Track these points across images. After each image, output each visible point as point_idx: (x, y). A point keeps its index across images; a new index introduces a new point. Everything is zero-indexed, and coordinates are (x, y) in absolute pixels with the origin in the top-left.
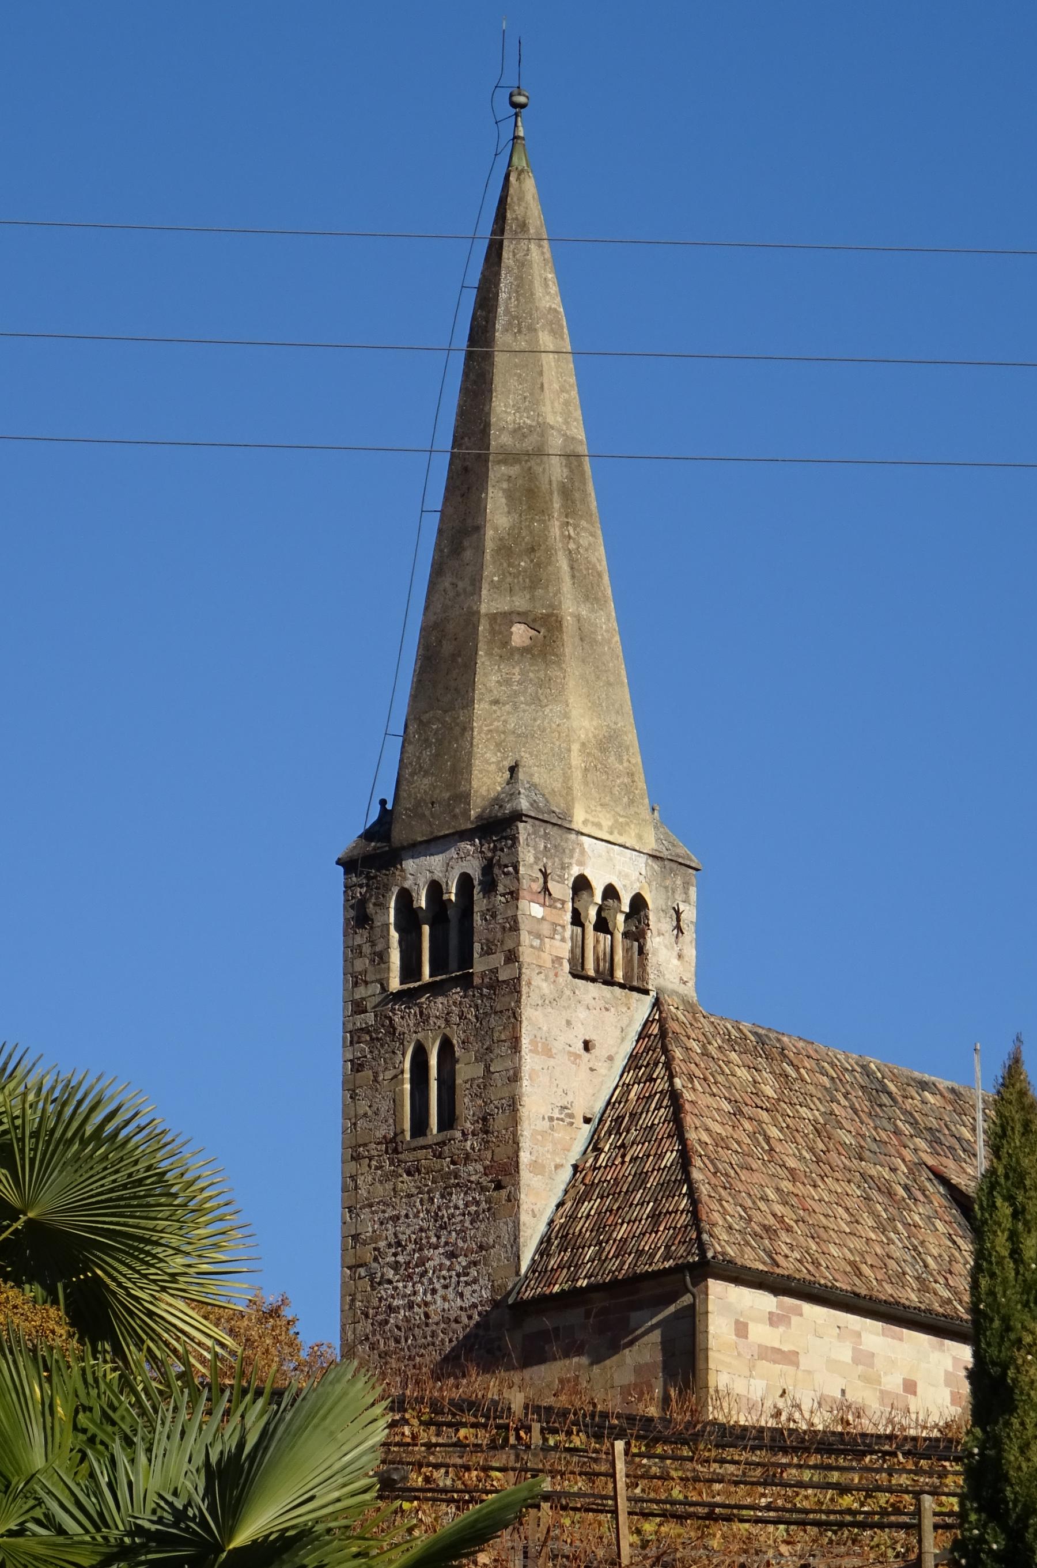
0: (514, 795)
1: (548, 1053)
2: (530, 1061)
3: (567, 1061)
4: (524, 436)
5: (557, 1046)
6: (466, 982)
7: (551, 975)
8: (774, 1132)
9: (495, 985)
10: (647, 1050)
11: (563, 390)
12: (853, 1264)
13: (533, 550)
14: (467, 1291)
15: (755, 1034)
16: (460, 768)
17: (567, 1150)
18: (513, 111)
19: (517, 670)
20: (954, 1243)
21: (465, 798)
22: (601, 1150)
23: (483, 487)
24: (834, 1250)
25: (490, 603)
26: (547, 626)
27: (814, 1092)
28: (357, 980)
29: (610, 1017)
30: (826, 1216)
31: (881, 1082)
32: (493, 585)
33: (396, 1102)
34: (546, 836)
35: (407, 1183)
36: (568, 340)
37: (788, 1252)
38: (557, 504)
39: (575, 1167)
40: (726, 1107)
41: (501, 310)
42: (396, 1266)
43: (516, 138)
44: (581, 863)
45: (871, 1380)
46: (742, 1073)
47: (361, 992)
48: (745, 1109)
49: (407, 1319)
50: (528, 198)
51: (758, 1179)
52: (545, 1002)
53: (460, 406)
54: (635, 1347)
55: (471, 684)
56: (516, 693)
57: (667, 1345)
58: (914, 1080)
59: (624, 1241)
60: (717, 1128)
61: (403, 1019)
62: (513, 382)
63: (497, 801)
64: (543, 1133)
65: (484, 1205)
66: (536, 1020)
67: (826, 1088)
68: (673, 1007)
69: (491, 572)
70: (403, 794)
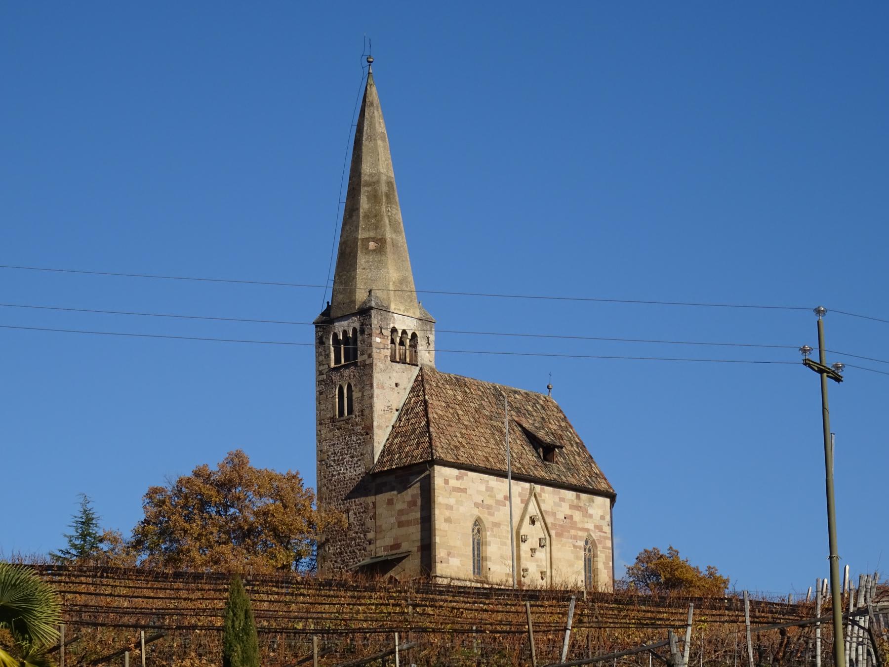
0: (370, 301)
1: (383, 388)
2: (376, 391)
3: (390, 390)
5: (387, 385)
8: (460, 412)
9: (365, 365)
16: (353, 292)
17: (390, 420)
21: (354, 302)
24: (480, 453)
25: (361, 235)
26: (381, 242)
28: (320, 363)
29: (405, 375)
33: (334, 405)
35: (337, 433)
40: (444, 404)
42: (334, 461)
46: (450, 392)
47: (321, 368)
51: (455, 430)
57: (422, 488)
59: (408, 452)
60: (440, 412)
61: (335, 377)
62: (369, 158)
63: (365, 303)
66: (378, 377)
68: (426, 370)
69: (362, 224)
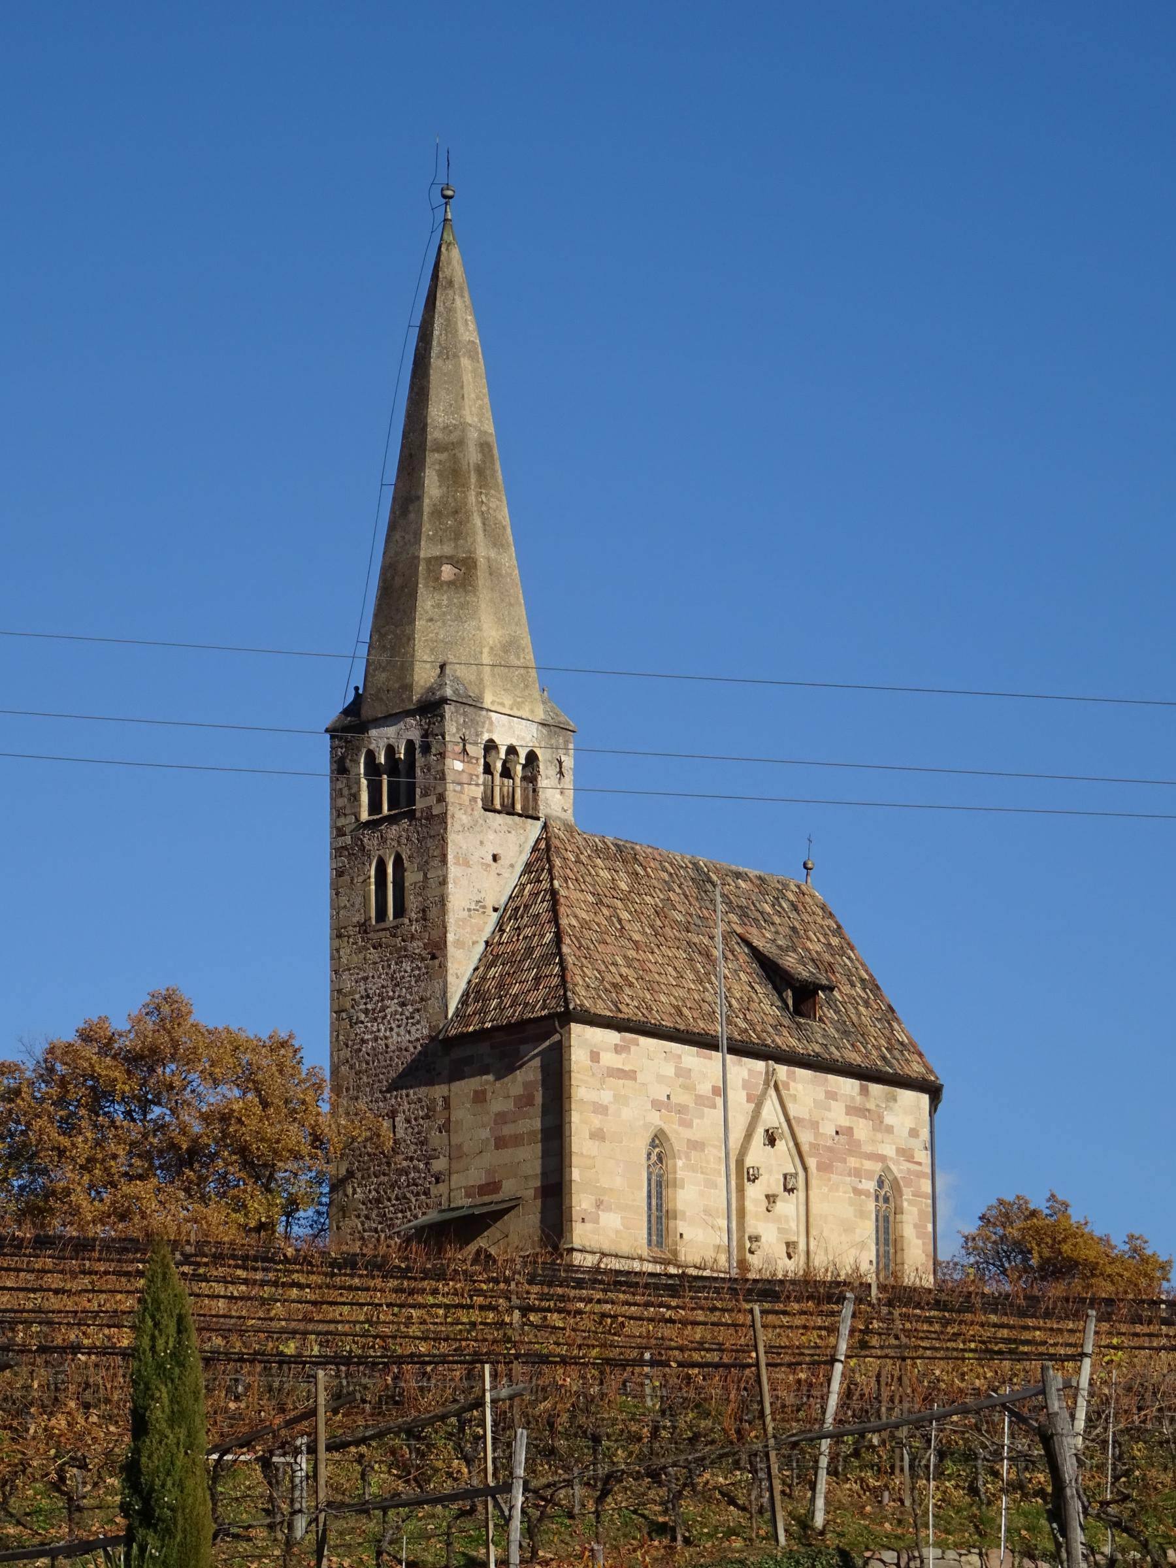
0: (442, 685)
1: (467, 864)
3: (480, 869)
4: (451, 432)
5: (474, 859)
6: (411, 815)
7: (469, 810)
8: (625, 915)
9: (430, 817)
10: (537, 860)
11: (478, 398)
12: (677, 1008)
13: (456, 512)
14: (413, 1029)
15: (616, 845)
16: (406, 668)
17: (481, 930)
18: (444, 201)
19: (445, 597)
20: (753, 988)
21: (409, 687)
22: (504, 931)
23: (422, 467)
24: (663, 998)
25: (426, 551)
26: (467, 565)
27: (656, 884)
28: (338, 812)
29: (512, 837)
30: (660, 974)
31: (707, 875)
32: (429, 538)
33: (366, 898)
34: (465, 714)
35: (373, 955)
36: (482, 362)
37: (629, 1001)
38: (473, 479)
39: (487, 942)
40: (591, 899)
41: (435, 343)
42: (366, 1012)
43: (445, 220)
44: (489, 731)
45: (688, 1088)
46: (605, 874)
47: (342, 822)
48: (605, 900)
49: (374, 1048)
50: (455, 263)
51: (613, 951)
52: (464, 829)
53: (407, 411)
54: (524, 1069)
55: (413, 608)
56: (444, 614)
57: (544, 1068)
58: (731, 871)
59: (516, 996)
60: (584, 915)
61: (370, 841)
62: (443, 393)
63: (431, 690)
64: (463, 920)
65: (424, 970)
66: (458, 841)
67: (665, 882)
69: (427, 529)
70: (369, 684)
